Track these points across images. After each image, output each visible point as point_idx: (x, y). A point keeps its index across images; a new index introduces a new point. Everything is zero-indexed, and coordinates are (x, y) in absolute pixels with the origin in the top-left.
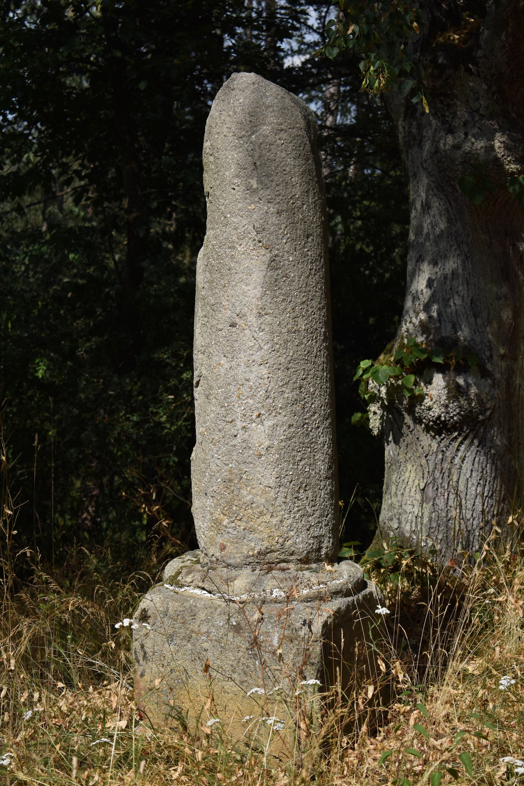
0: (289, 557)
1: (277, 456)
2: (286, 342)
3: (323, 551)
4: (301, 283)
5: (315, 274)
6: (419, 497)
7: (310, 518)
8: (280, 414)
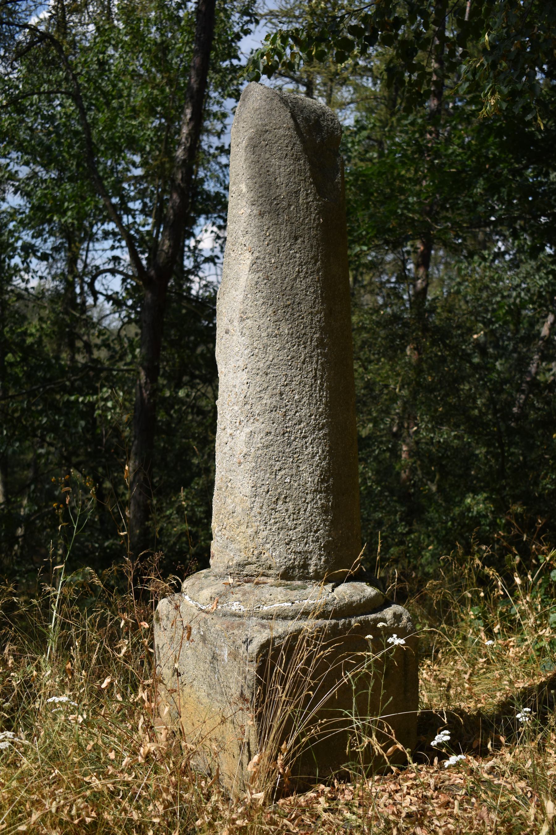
0: (267, 571)
1: (254, 464)
2: (265, 346)
3: (312, 569)
4: (285, 285)
5: (305, 277)
7: (291, 532)
8: (258, 420)
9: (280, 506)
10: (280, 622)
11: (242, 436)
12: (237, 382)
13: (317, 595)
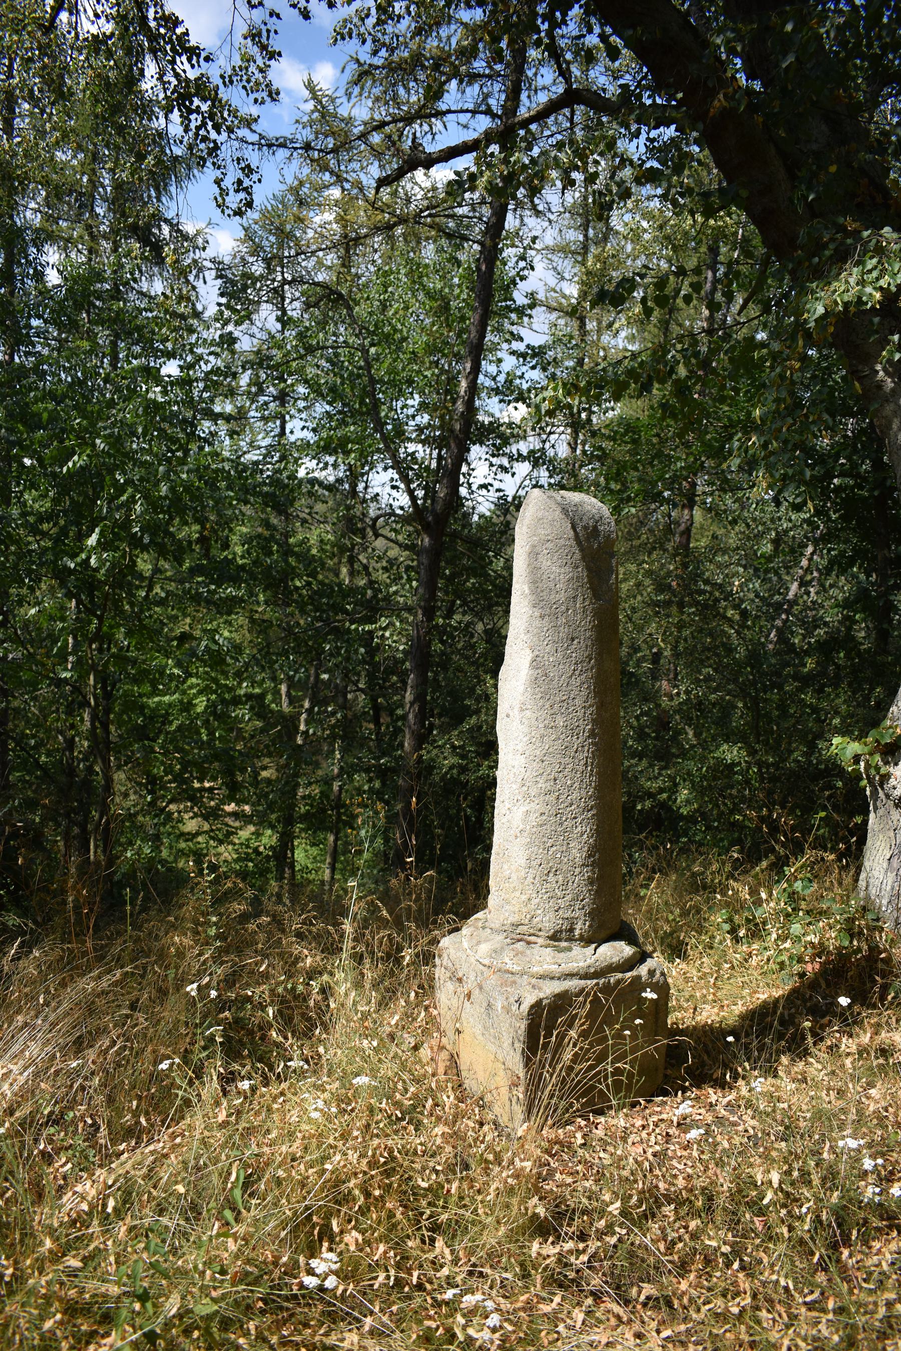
2: (542, 736)
3: (577, 932)
6: (885, 865)
9: (551, 878)
10: (548, 982)
11: (519, 812)
12: (516, 763)
13: (583, 957)
